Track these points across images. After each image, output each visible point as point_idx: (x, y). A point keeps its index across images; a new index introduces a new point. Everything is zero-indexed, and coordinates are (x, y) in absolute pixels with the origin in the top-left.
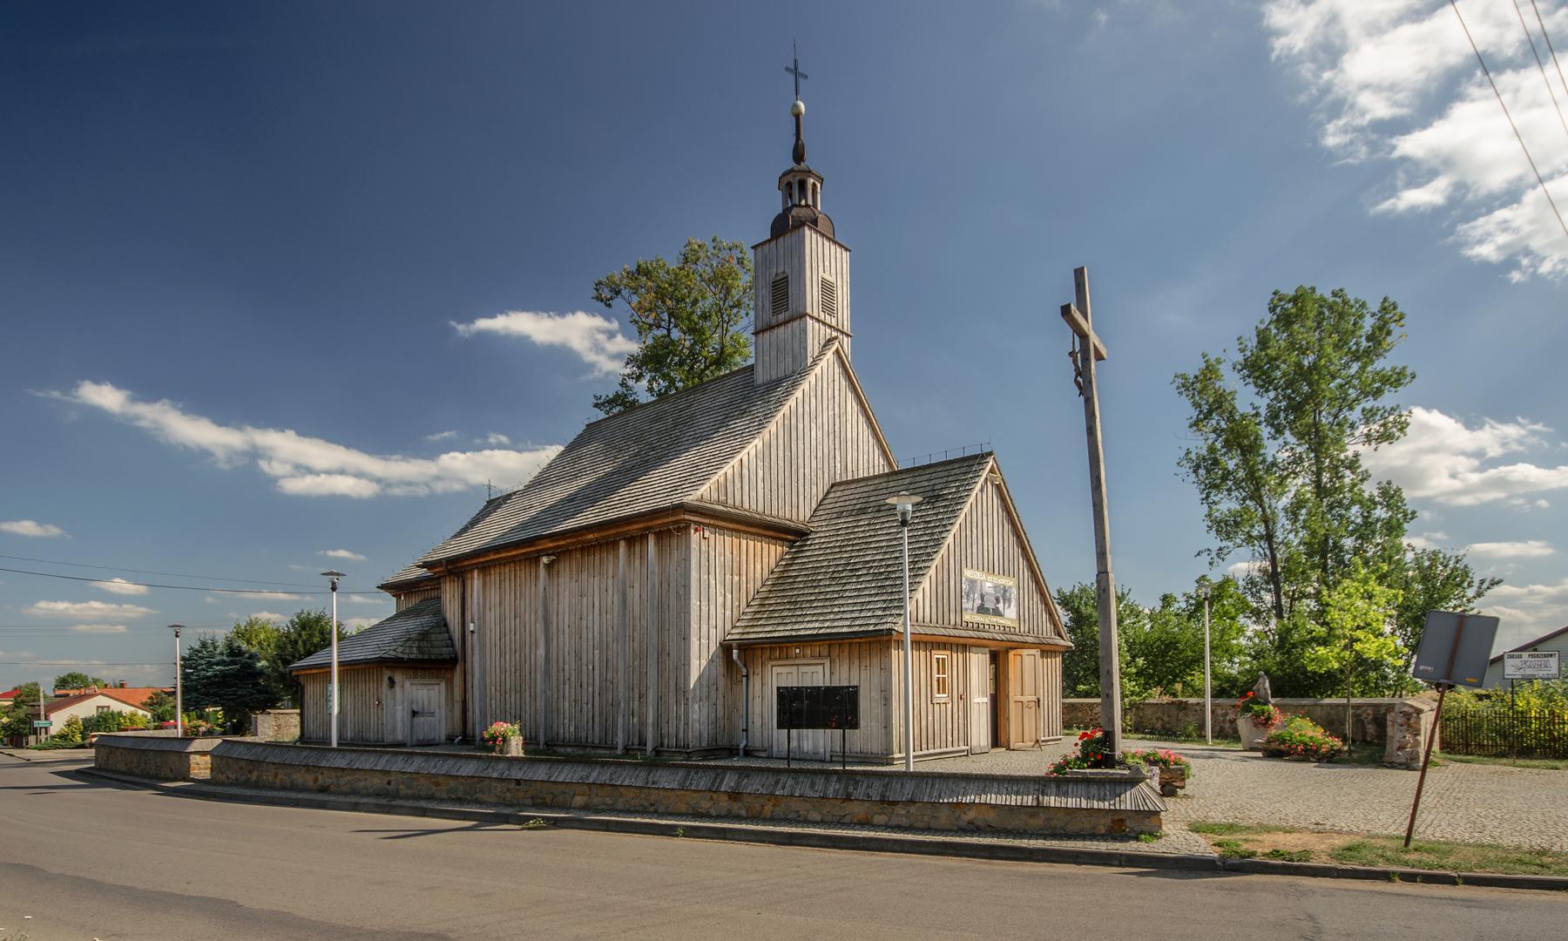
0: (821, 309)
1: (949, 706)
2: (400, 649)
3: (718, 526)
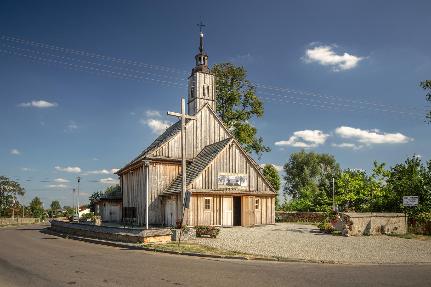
0: (203, 95)
1: (212, 213)
2: (107, 196)
3: (159, 163)
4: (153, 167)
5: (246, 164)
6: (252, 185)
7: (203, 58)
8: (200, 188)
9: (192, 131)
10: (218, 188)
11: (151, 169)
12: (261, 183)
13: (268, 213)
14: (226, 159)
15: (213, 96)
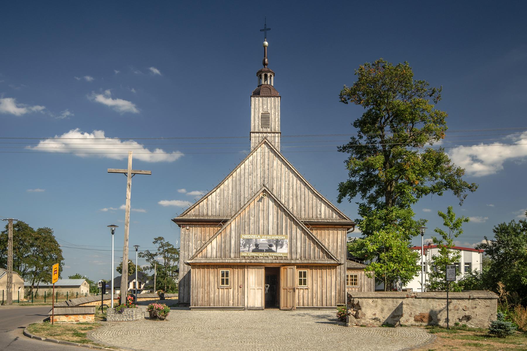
0: (260, 127)
1: (231, 290)
4: (186, 230)
5: (285, 221)
6: (295, 250)
7: (264, 75)
8: (212, 256)
9: (243, 179)
10: (241, 255)
11: (184, 233)
12: (312, 248)
13: (324, 291)
14: (253, 216)
15: (276, 126)
